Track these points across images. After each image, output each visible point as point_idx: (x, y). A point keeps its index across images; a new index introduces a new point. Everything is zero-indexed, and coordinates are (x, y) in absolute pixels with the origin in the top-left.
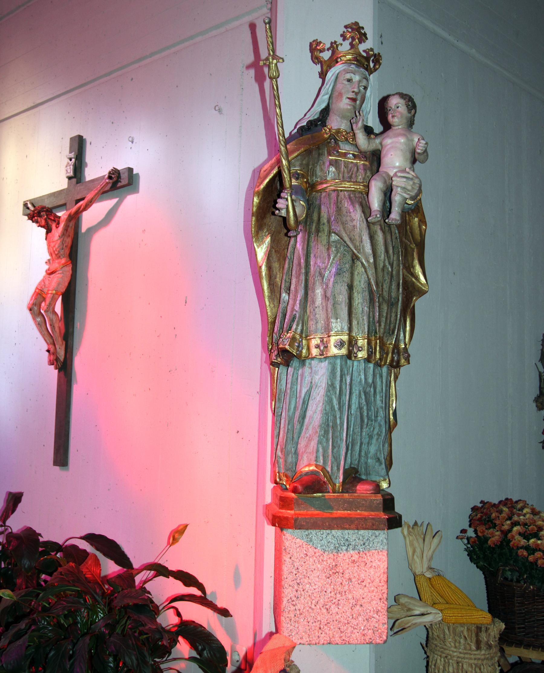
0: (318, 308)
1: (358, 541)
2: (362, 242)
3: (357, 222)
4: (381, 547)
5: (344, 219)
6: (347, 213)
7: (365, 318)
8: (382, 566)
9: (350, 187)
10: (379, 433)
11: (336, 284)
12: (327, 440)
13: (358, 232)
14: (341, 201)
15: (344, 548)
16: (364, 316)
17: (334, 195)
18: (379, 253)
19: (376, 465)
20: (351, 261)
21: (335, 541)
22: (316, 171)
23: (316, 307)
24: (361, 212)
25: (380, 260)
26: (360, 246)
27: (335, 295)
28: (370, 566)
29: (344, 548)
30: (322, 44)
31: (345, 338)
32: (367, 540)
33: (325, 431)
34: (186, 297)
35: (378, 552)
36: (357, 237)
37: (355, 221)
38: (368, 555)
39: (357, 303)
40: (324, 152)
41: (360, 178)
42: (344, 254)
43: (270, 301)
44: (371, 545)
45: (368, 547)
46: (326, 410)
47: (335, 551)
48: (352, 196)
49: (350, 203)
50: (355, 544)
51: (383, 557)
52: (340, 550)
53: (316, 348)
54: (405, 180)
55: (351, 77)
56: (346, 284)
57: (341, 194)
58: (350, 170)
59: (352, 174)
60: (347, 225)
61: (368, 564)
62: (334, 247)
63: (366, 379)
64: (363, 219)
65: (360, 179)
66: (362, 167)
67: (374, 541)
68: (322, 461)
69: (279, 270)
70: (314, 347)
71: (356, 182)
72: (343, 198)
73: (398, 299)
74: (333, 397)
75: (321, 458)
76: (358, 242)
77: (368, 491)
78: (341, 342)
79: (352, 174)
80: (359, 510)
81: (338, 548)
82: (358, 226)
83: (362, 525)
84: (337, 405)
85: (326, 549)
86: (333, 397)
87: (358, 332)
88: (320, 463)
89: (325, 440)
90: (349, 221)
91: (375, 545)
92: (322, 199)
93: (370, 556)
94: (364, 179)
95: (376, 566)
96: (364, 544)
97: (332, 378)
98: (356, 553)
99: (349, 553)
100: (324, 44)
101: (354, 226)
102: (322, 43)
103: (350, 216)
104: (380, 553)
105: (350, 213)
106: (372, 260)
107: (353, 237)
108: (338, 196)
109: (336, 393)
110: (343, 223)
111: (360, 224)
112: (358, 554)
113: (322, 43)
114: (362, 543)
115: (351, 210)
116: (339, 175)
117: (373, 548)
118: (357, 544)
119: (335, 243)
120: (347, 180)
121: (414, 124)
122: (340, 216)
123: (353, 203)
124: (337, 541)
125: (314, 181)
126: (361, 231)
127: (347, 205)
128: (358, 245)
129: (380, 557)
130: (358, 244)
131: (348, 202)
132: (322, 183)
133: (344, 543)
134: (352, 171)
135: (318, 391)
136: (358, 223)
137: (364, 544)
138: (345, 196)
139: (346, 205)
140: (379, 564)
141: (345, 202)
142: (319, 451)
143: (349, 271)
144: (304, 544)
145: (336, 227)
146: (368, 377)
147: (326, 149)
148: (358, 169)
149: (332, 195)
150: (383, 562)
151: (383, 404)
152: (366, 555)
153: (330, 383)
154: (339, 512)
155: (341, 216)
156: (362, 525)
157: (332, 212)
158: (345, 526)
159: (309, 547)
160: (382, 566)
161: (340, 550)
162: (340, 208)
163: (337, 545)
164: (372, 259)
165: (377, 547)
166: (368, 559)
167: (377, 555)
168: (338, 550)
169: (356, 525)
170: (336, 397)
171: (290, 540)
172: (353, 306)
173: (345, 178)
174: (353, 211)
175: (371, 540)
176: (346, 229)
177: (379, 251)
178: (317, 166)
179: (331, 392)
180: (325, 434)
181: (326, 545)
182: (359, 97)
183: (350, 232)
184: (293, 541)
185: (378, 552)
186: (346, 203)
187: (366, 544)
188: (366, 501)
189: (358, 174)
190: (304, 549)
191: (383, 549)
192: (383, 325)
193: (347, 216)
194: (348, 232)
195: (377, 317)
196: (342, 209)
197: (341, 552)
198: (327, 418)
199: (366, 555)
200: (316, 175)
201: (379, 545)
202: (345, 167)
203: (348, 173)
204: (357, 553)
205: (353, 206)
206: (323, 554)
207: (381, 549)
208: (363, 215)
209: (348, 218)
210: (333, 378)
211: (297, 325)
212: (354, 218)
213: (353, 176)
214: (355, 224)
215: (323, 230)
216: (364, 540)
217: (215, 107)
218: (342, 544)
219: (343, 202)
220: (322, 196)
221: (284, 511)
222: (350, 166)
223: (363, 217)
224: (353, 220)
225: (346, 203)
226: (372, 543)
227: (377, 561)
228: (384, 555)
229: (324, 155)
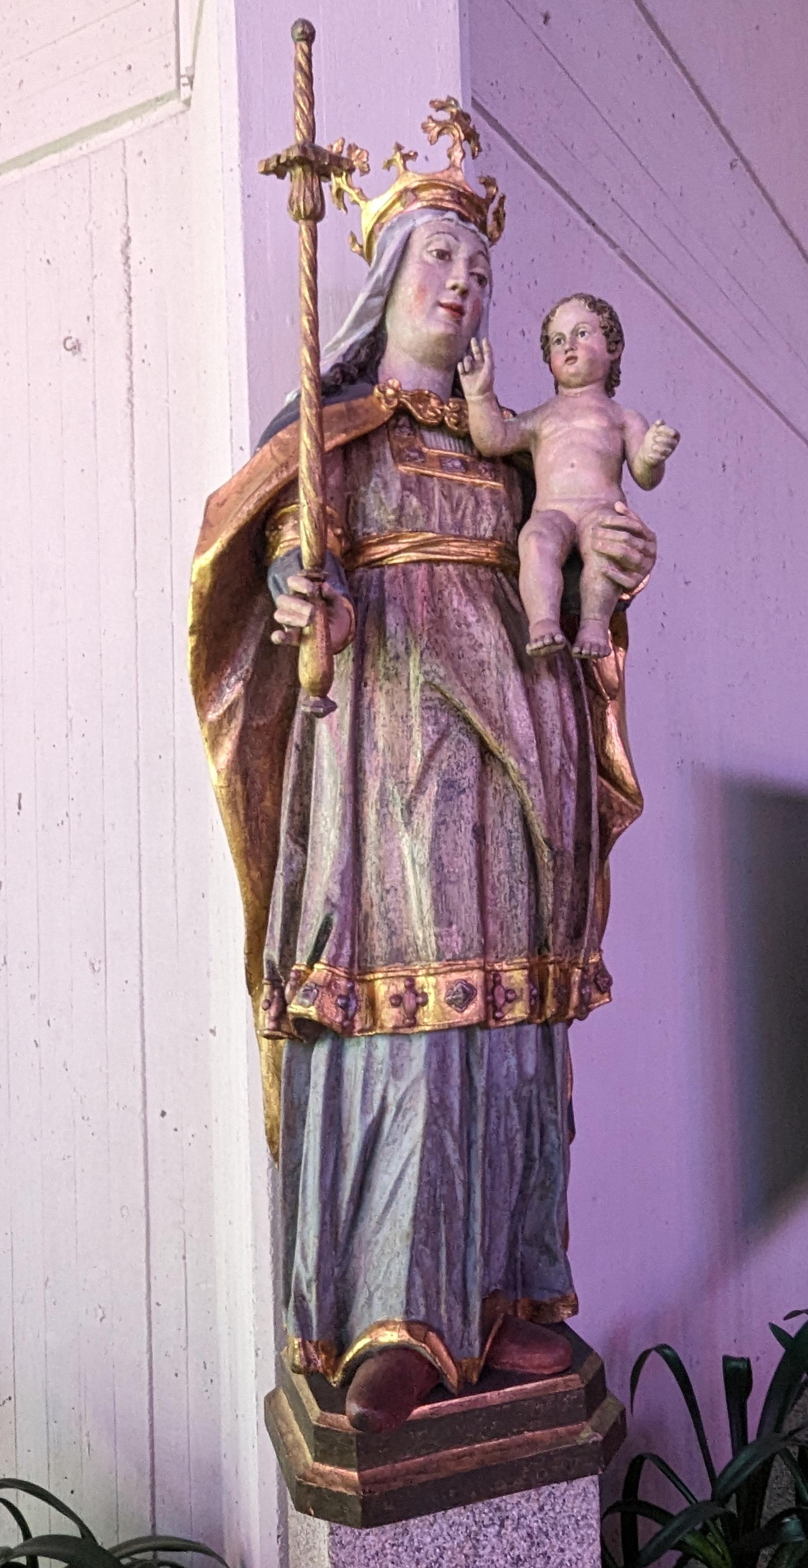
0: (392, 892)
1: (526, 1505)
2: (506, 707)
3: (489, 653)
4: (585, 1506)
5: (454, 642)
6: (460, 626)
7: (519, 911)
8: (586, 1556)
9: (463, 554)
10: (548, 1183)
11: (443, 827)
12: (436, 1251)
13: (493, 680)
14: (441, 592)
15: (493, 1530)
16: (516, 907)
17: (420, 574)
18: (549, 734)
19: (539, 1261)
20: (479, 760)
21: (468, 1518)
22: (364, 505)
23: (388, 891)
24: (499, 623)
25: (551, 753)
26: (502, 719)
27: (440, 858)
28: (558, 1561)
29: (493, 1530)
30: (358, 152)
31: (476, 977)
32: (549, 1495)
33: (428, 1229)
34: (20, 796)
35: (577, 1521)
36: (492, 694)
37: (484, 649)
38: (552, 1533)
39: (496, 874)
40: (384, 454)
41: (486, 527)
42: (459, 741)
43: (250, 860)
44: (558, 1509)
45: (551, 1514)
46: (429, 1174)
47: (470, 1544)
48: (468, 577)
49: (465, 598)
50: (519, 1514)
51: (589, 1532)
52: (482, 1538)
53: (395, 1005)
54: (624, 535)
55: (448, 245)
56: (470, 827)
57: (439, 569)
58: (458, 505)
59: (463, 516)
60: (462, 661)
61: (552, 1559)
62: (432, 721)
63: (520, 1065)
64: (505, 644)
65: (485, 530)
66: (486, 497)
67: (565, 1496)
68: (423, 1310)
69: (271, 777)
70: (387, 1003)
71: (476, 539)
72: (445, 583)
73: (589, 846)
74: (446, 1133)
75: (421, 1301)
76: (496, 707)
77: (545, 1368)
78: (465, 991)
79: (463, 516)
80: (529, 1431)
81: (477, 1534)
82: (494, 661)
83: (541, 1474)
84: (454, 1152)
85: (446, 1545)
86: (446, 1133)
87: (502, 952)
88: (418, 1313)
89: (428, 1251)
90: (465, 648)
91: (570, 1505)
92: (387, 585)
93: (557, 1535)
94: (495, 530)
95: (574, 1559)
96: (541, 1509)
97: (440, 1085)
98: (522, 1538)
99: (504, 1541)
100: (362, 150)
101: (482, 663)
102: (357, 148)
103: (469, 634)
104: (581, 1523)
105: (468, 625)
106: (534, 759)
107: (481, 695)
108: (431, 575)
109: (451, 1124)
110: (451, 657)
111: (497, 656)
112: (528, 1539)
113: (357, 148)
114: (536, 1507)
115: (472, 619)
116: (428, 519)
117: (563, 1514)
118: (524, 1511)
119: (433, 712)
120: (453, 532)
121: (618, 382)
122: (443, 637)
123: (473, 600)
124: (474, 1516)
125: (360, 534)
126: (503, 676)
127: (460, 603)
128: (498, 716)
129: (582, 1532)
130: (495, 713)
131: (460, 595)
132: (475, 563)
133: (491, 1519)
134: (462, 507)
135: (405, 1123)
136: (493, 654)
137: (541, 1509)
138: (449, 578)
139: (455, 604)
140: (579, 1551)
141: (450, 593)
142: (414, 1284)
143: (475, 789)
144: (387, 1546)
145: (434, 667)
146: (524, 1057)
147: (388, 444)
148: (478, 504)
149: (414, 575)
150: (590, 1544)
151: (557, 1113)
152: (547, 1535)
153: (436, 1100)
154: (477, 1446)
155: (446, 636)
156: (541, 1474)
157: (419, 622)
158: (499, 1489)
159: (400, 1549)
160: (586, 1556)
161: (482, 1538)
162: (441, 611)
163: (474, 1528)
164: (536, 754)
165: (573, 1509)
166: (552, 1547)
167: (574, 1530)
168: (478, 1540)
169: (525, 1480)
170: (452, 1132)
171: (349, 1543)
172: (488, 880)
173: (447, 529)
174: (478, 621)
175: (558, 1494)
176: (462, 672)
177: (548, 728)
178: (366, 493)
179: (441, 1121)
180: (427, 1235)
181: (445, 1533)
182: (468, 306)
183: (473, 680)
184: (358, 1542)
185: (577, 1521)
186: (455, 598)
187: (546, 1508)
188: (544, 1402)
189: (479, 517)
190: (389, 1557)
191: (588, 1510)
192: (562, 923)
193: (461, 636)
194: (466, 679)
195: (550, 907)
196: (445, 614)
197: (485, 1542)
198: (432, 1193)
199: (547, 1535)
200: (365, 517)
201: (578, 1502)
202: (445, 497)
203: (454, 511)
204: (525, 1535)
205: (475, 606)
206: (440, 1560)
207: (584, 1512)
208: (503, 631)
209: (465, 641)
210: (443, 1083)
211: (339, 946)
212: (481, 641)
213: (468, 521)
214: (486, 659)
215: (396, 674)
216: (541, 1499)
217: (65, 340)
218: (486, 1522)
219: (446, 593)
220: (386, 577)
221: (328, 1468)
222: (456, 493)
223: (506, 638)
224: (477, 646)
225: (455, 598)
226: (561, 1501)
227: (574, 1544)
228: (590, 1526)
229: (385, 462)
